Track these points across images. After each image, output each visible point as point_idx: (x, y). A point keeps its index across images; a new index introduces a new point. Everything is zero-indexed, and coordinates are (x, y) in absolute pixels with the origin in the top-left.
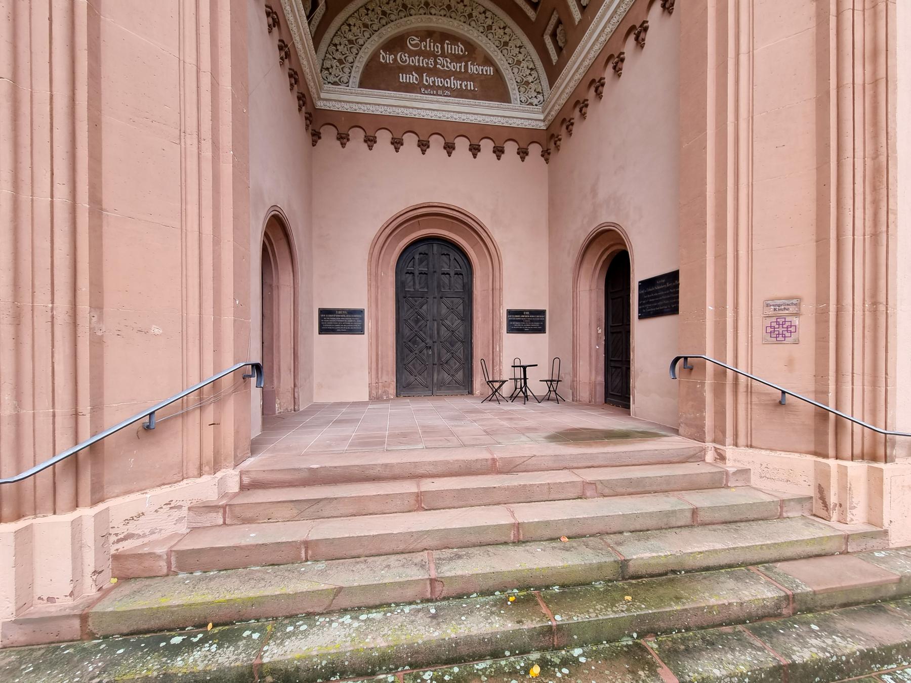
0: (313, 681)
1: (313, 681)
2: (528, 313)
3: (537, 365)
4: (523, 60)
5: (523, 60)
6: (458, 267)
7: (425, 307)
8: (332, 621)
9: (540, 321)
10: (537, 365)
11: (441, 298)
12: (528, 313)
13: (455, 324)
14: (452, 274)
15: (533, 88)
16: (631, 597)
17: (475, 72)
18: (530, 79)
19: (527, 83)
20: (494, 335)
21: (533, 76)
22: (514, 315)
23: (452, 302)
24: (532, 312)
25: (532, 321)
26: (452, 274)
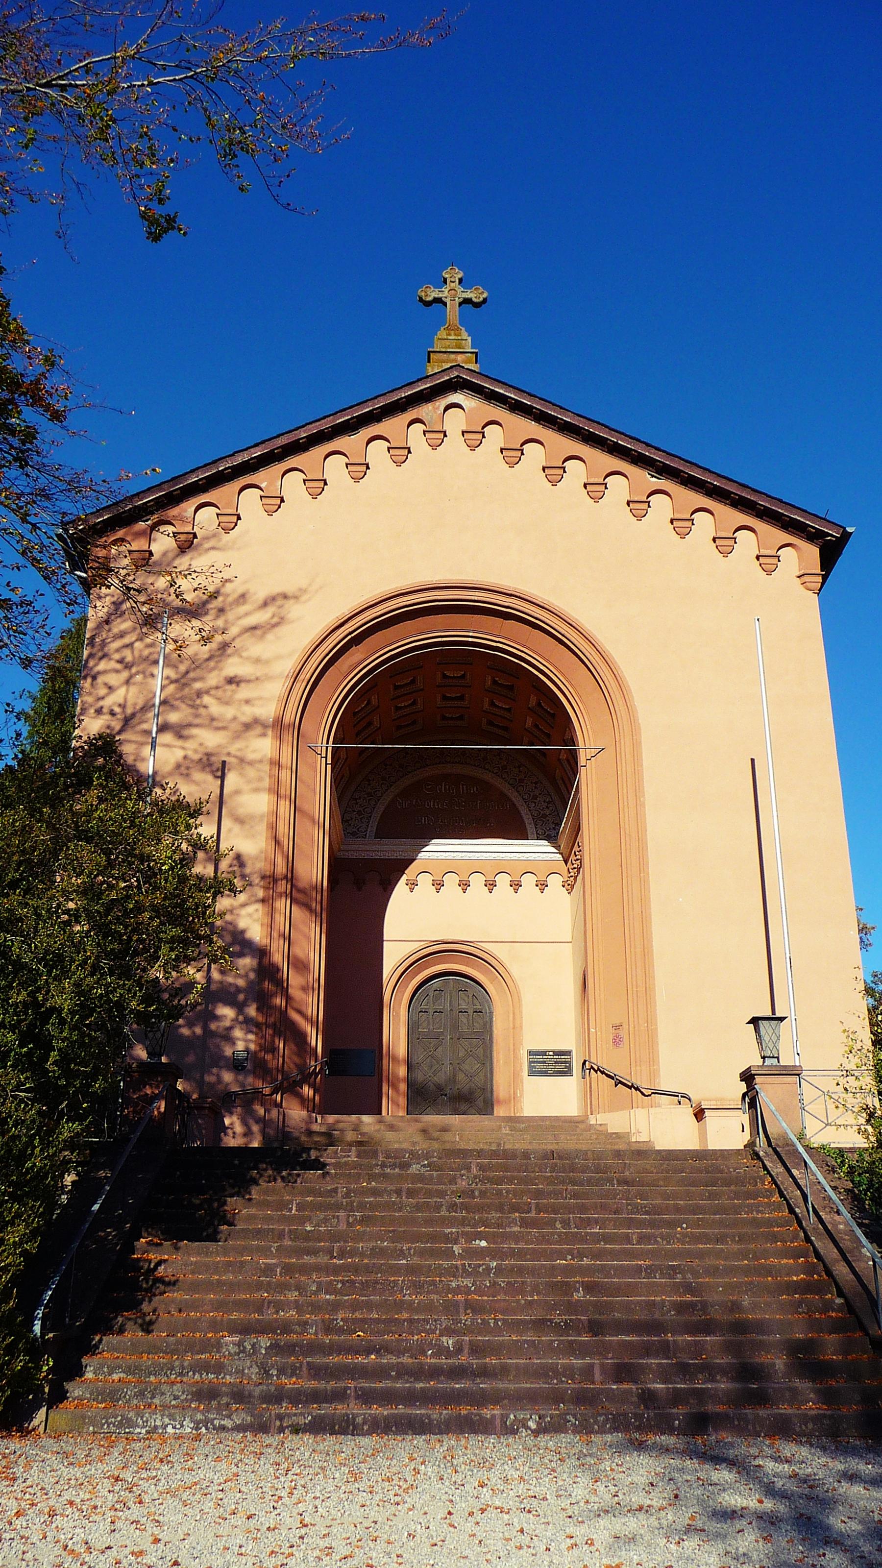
0: (59, 1566)
1: (59, 1566)
2: (551, 1053)
3: (753, 760)
4: (540, 794)
5: (540, 794)
6: (478, 1004)
7: (440, 1049)
8: (175, 1345)
9: (565, 1062)
10: (753, 760)
11: (458, 1039)
12: (551, 1053)
13: (474, 1069)
14: (471, 1012)
15: (551, 820)
16: (836, 1302)
17: (446, 1344)
18: (547, 812)
19: (545, 816)
20: (516, 1077)
21: (551, 808)
22: (536, 1055)
23: (470, 1044)
24: (544, 1073)
25: (556, 1062)
26: (471, 1012)
